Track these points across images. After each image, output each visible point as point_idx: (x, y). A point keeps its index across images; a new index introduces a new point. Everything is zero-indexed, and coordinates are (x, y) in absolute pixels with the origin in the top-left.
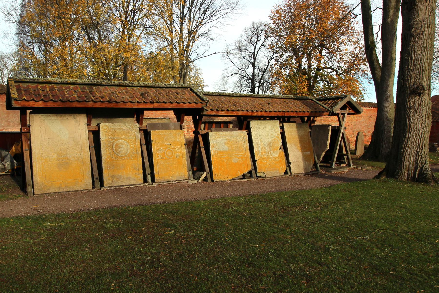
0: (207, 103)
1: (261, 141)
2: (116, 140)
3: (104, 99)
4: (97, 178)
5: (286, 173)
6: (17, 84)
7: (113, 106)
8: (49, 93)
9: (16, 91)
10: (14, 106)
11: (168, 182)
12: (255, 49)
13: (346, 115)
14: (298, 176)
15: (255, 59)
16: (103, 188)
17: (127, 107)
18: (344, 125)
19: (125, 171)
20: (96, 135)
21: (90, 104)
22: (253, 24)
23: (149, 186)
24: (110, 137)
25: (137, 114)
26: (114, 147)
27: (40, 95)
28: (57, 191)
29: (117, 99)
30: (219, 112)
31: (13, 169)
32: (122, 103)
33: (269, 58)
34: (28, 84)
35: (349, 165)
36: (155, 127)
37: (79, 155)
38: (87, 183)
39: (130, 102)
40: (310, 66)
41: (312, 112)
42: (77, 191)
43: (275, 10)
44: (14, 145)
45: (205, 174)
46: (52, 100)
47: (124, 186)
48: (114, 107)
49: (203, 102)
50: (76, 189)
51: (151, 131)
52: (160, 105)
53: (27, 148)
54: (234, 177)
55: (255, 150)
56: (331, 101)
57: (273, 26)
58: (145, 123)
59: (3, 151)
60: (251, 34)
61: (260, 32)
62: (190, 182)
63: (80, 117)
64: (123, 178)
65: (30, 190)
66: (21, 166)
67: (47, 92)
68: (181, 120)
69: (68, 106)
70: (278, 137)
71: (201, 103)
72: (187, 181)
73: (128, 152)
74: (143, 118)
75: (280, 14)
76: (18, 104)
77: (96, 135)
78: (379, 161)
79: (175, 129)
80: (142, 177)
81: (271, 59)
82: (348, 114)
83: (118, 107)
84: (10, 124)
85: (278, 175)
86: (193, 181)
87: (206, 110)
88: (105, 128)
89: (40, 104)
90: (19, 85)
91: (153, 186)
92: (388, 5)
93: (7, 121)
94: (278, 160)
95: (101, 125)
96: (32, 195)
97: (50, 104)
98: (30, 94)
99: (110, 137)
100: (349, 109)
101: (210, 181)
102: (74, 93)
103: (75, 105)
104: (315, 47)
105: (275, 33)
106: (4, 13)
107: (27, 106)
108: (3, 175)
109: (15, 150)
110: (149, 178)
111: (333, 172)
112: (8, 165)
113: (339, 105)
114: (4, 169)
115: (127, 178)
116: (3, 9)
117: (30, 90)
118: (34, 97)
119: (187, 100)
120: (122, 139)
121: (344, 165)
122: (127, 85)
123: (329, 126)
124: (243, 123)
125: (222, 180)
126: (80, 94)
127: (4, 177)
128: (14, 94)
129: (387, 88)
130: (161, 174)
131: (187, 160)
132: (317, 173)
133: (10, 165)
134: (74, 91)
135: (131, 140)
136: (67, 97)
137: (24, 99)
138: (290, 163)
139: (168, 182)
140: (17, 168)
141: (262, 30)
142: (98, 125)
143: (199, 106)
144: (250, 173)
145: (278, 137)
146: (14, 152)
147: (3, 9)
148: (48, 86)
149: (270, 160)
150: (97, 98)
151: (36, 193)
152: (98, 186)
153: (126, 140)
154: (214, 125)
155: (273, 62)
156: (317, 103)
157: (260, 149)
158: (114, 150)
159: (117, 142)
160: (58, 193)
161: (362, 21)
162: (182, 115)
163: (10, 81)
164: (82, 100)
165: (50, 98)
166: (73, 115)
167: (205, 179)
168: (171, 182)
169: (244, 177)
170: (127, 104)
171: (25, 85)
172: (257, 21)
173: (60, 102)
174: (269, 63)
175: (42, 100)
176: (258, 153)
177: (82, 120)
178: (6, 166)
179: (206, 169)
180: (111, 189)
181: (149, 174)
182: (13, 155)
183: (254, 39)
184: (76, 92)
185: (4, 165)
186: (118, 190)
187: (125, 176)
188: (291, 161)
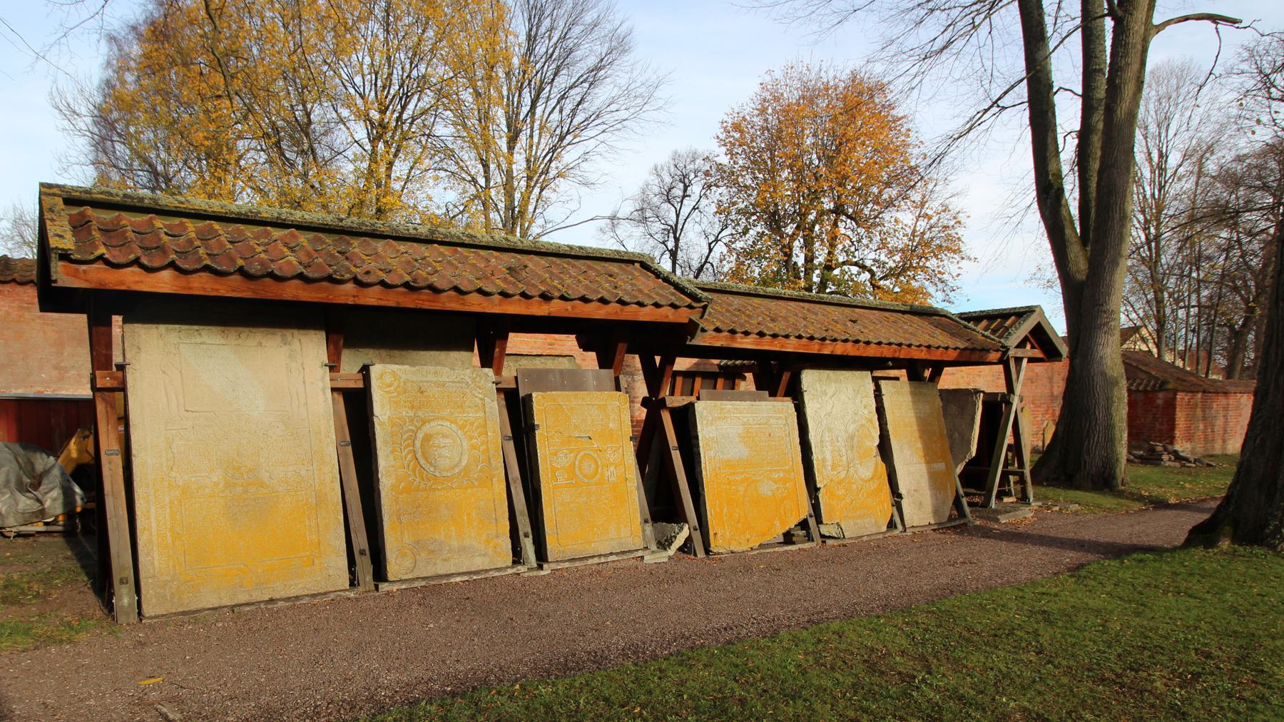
0: (705, 308)
1: (830, 430)
2: (424, 422)
3: (392, 274)
4: (362, 553)
5: (892, 525)
6: (75, 211)
7: (423, 301)
8: (197, 243)
9: (68, 228)
10: (60, 284)
11: (586, 558)
12: (678, 216)
13: (1025, 361)
14: (920, 533)
15: (677, 240)
16: (384, 587)
17: (466, 309)
18: (1018, 389)
19: (452, 525)
20: (357, 406)
21: (346, 294)
22: (676, 156)
23: (531, 574)
24: (406, 413)
25: (484, 334)
26: (418, 444)
27: (161, 249)
28: (226, 601)
29: (434, 280)
30: (733, 339)
31: (70, 514)
32: (453, 293)
33: (712, 238)
34: (117, 213)
35: (1024, 498)
36: (543, 380)
37: (303, 473)
38: (330, 569)
39: (480, 291)
40: (809, 259)
41: (966, 349)
42: (297, 598)
43: (730, 121)
44: (68, 433)
45: (685, 533)
46: (207, 268)
47: (452, 575)
48: (427, 306)
49: (694, 304)
50: (293, 592)
51: (534, 395)
52: (568, 305)
53: (116, 447)
54: (764, 540)
55: (815, 457)
56: (984, 323)
57: (724, 160)
58: (510, 369)
59: (38, 455)
60: (668, 180)
61: (692, 176)
62: (649, 559)
63: (304, 339)
64: (449, 551)
65: (126, 601)
66: (92, 505)
67: (190, 241)
68: (616, 361)
69: (269, 296)
70: (871, 421)
71: (690, 307)
72: (640, 554)
73: (464, 463)
74: (503, 354)
75: (742, 132)
76: (76, 275)
77: (357, 406)
78: (1078, 488)
79: (599, 388)
80: (507, 544)
81: (717, 240)
82: (1031, 360)
83: (437, 306)
84: (51, 360)
85: (874, 530)
86: (657, 555)
87: (703, 330)
88: (388, 379)
89: (164, 282)
90: (82, 214)
91: (542, 573)
92: (1120, 69)
93: (56, 367)
94: (873, 485)
95: (375, 371)
96: (134, 618)
97: (201, 285)
98: (125, 244)
99: (406, 413)
100: (1033, 347)
101: (701, 554)
102: (285, 249)
103: (293, 291)
104: (821, 213)
105: (727, 176)
106: (57, 108)
107: (111, 286)
108: (38, 532)
109: (80, 452)
110: (528, 546)
111: (1003, 519)
112: (53, 500)
113: (1018, 332)
114: (42, 513)
115: (463, 550)
116: (57, 100)
117: (125, 232)
118: (139, 252)
119: (650, 297)
120: (442, 418)
121: (1012, 499)
122: (455, 240)
123: (977, 392)
124: (779, 374)
125: (733, 548)
126: (309, 255)
127: (42, 539)
128: (60, 236)
129: (1109, 294)
130: (568, 532)
131: (638, 489)
132: (965, 524)
133: (60, 501)
134: (286, 245)
135: (472, 424)
136: (262, 263)
137: (101, 258)
138: (900, 496)
139: (586, 558)
140: (84, 510)
141: (696, 172)
142: (365, 371)
143: (683, 316)
144: (804, 525)
145: (871, 421)
146: (72, 459)
147: (57, 100)
148: (191, 226)
149: (854, 486)
150: (368, 273)
151: (148, 610)
152: (369, 578)
153: (455, 422)
154: (698, 381)
155: (720, 249)
156: (965, 327)
157: (828, 457)
158: (419, 455)
159: (427, 428)
160: (232, 608)
161: (1030, 118)
162: (622, 346)
163: (46, 194)
164: (316, 275)
165: (200, 259)
166: (279, 332)
167: (687, 548)
168: (596, 560)
169: (788, 538)
170: (466, 297)
171: (107, 216)
172: (683, 150)
173: (237, 277)
174: (711, 250)
175: (172, 265)
176: (824, 466)
177: (310, 349)
178: (47, 504)
179: (688, 514)
180: (412, 589)
181: (526, 536)
182: (69, 470)
183: (678, 192)
184: (292, 249)
185: (38, 500)
186: (433, 591)
187: (455, 543)
188: (902, 490)
